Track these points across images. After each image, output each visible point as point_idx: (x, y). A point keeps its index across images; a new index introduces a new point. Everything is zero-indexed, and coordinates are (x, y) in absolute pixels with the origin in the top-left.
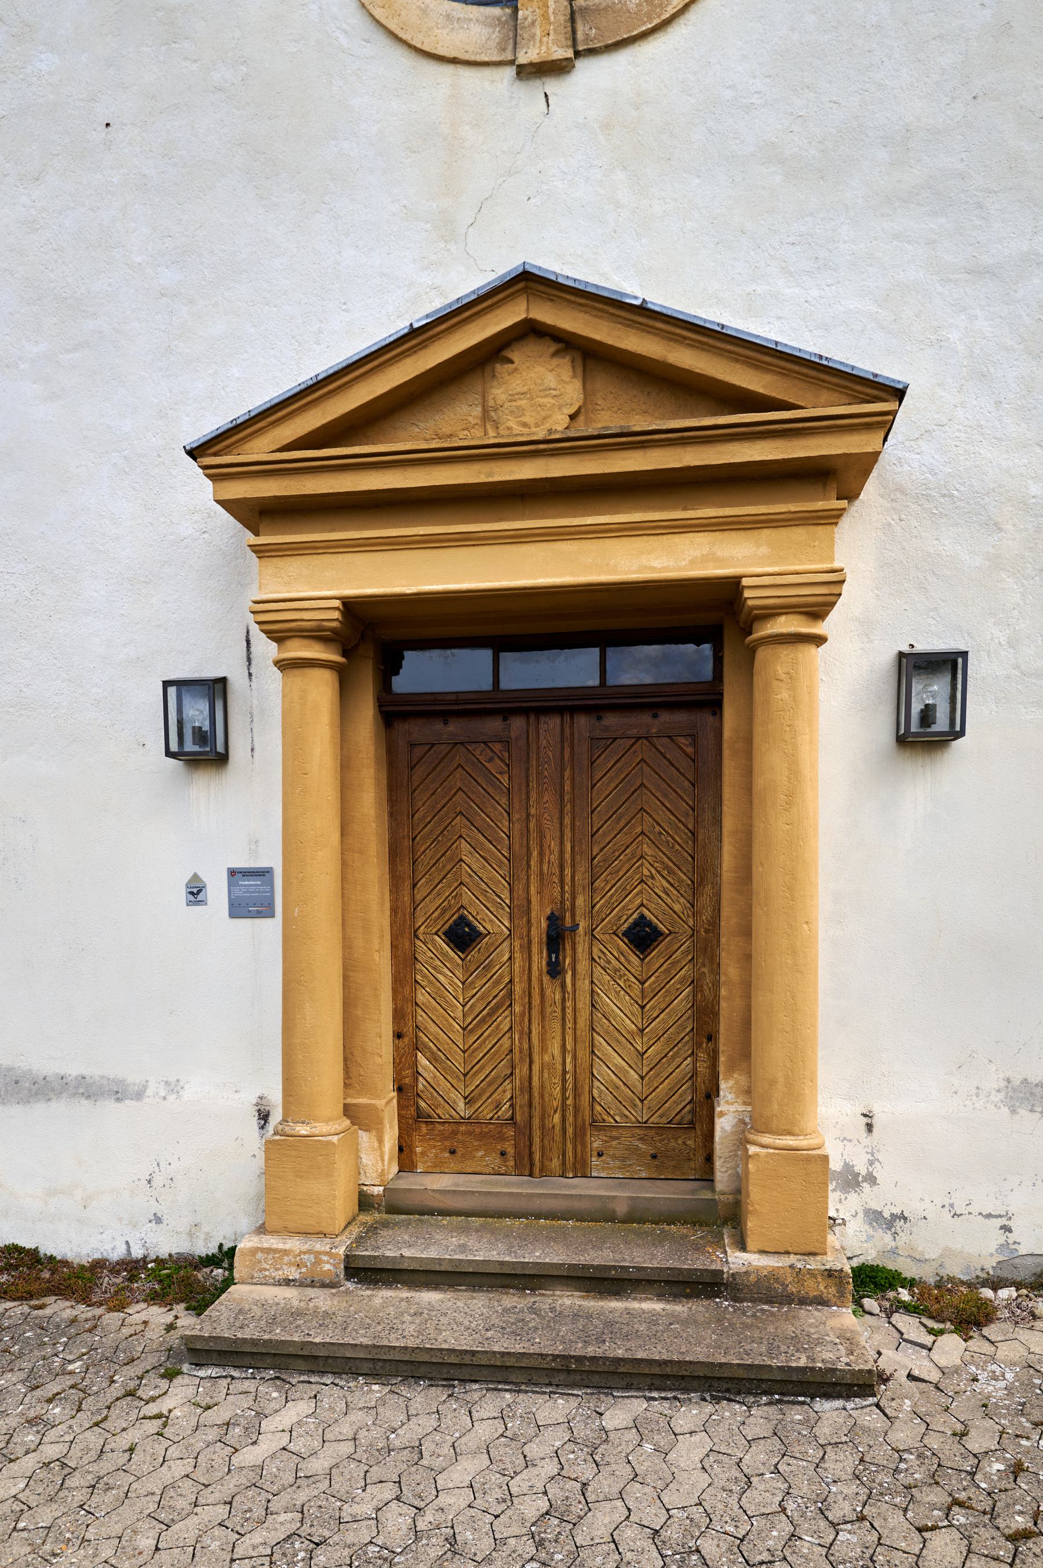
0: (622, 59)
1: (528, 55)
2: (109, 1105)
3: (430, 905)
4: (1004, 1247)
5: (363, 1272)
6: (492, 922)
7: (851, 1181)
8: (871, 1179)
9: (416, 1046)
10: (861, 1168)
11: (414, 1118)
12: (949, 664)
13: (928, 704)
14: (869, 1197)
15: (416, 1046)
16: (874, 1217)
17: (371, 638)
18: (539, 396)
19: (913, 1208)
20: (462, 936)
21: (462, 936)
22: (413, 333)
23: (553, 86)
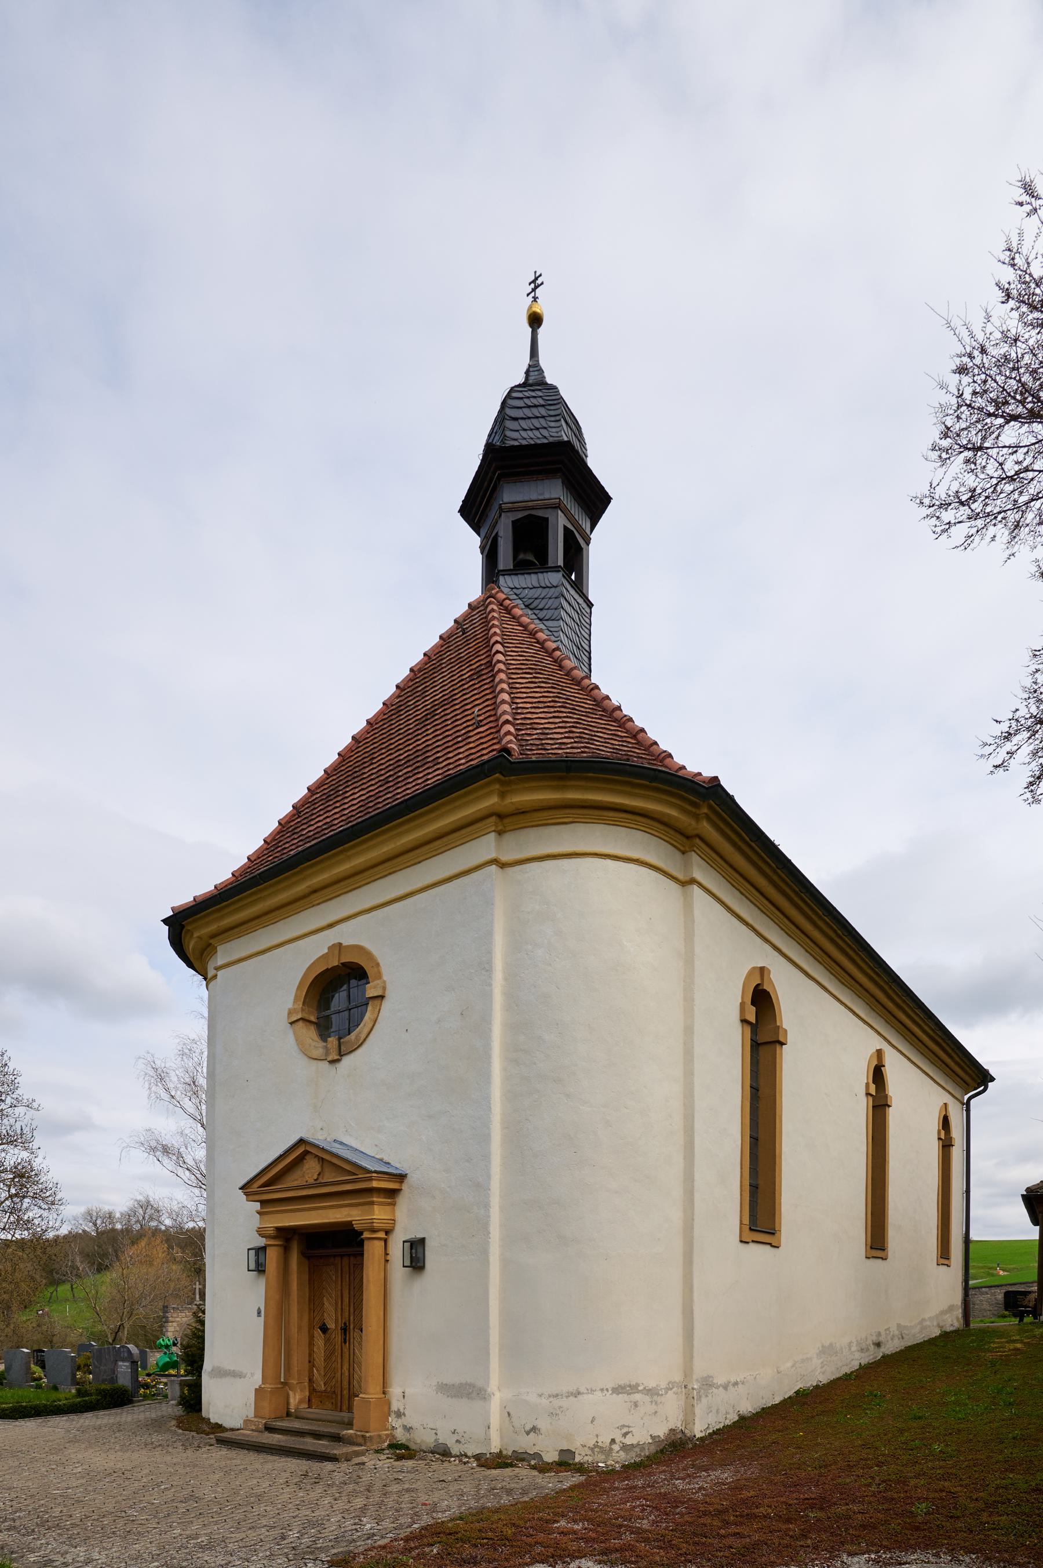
0: (352, 1055)
1: (330, 1058)
2: (238, 1379)
3: (317, 1319)
4: (436, 1440)
5: (269, 1429)
6: (331, 1325)
7: (399, 1414)
8: (404, 1414)
9: (314, 1366)
10: (402, 1411)
11: (313, 1390)
12: (422, 1241)
13: (416, 1255)
14: (403, 1421)
15: (314, 1366)
16: (405, 1427)
17: (286, 1235)
18: (310, 1170)
19: (415, 1425)
20: (324, 1329)
21: (324, 1329)
22: (281, 1156)
23: (338, 1065)
